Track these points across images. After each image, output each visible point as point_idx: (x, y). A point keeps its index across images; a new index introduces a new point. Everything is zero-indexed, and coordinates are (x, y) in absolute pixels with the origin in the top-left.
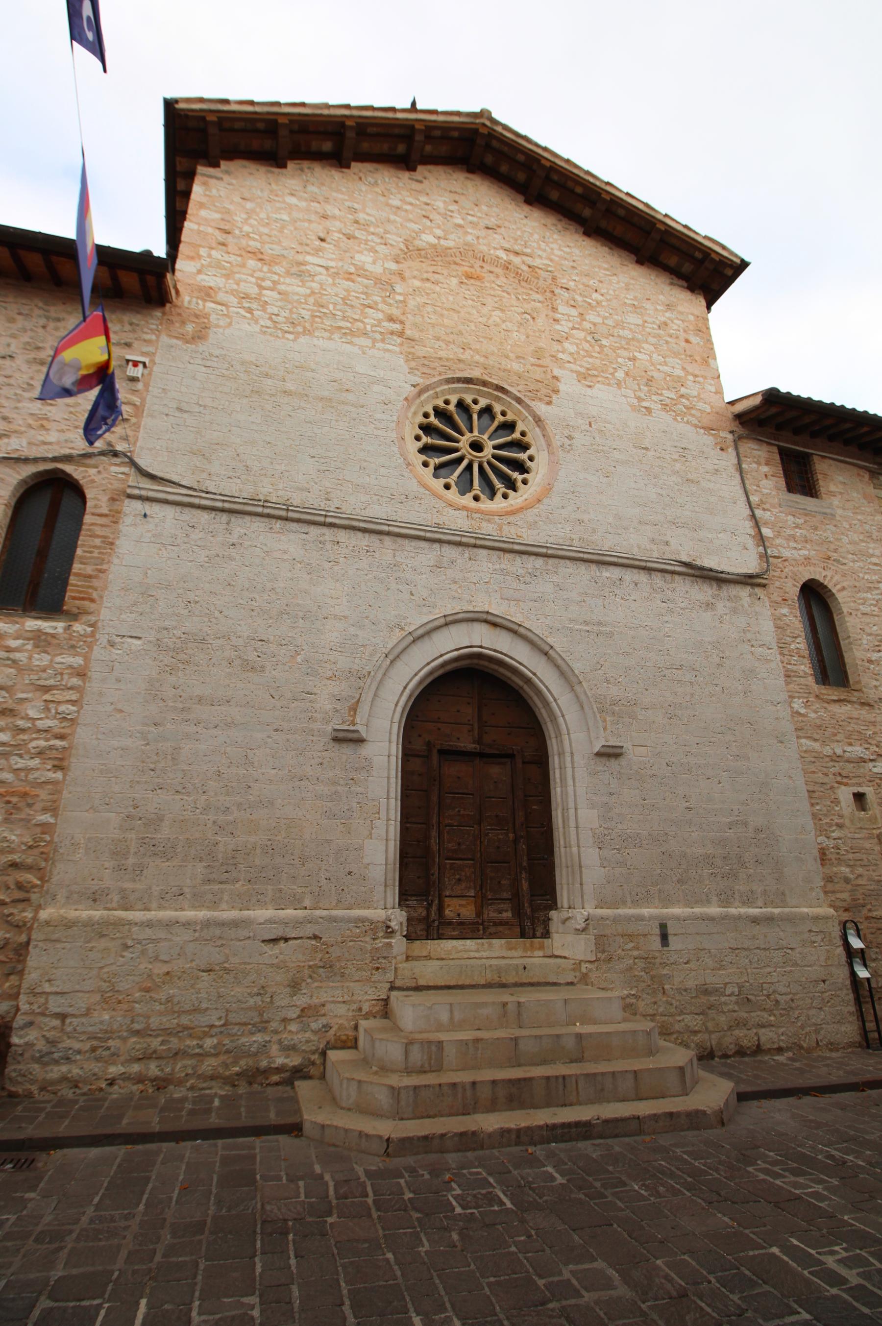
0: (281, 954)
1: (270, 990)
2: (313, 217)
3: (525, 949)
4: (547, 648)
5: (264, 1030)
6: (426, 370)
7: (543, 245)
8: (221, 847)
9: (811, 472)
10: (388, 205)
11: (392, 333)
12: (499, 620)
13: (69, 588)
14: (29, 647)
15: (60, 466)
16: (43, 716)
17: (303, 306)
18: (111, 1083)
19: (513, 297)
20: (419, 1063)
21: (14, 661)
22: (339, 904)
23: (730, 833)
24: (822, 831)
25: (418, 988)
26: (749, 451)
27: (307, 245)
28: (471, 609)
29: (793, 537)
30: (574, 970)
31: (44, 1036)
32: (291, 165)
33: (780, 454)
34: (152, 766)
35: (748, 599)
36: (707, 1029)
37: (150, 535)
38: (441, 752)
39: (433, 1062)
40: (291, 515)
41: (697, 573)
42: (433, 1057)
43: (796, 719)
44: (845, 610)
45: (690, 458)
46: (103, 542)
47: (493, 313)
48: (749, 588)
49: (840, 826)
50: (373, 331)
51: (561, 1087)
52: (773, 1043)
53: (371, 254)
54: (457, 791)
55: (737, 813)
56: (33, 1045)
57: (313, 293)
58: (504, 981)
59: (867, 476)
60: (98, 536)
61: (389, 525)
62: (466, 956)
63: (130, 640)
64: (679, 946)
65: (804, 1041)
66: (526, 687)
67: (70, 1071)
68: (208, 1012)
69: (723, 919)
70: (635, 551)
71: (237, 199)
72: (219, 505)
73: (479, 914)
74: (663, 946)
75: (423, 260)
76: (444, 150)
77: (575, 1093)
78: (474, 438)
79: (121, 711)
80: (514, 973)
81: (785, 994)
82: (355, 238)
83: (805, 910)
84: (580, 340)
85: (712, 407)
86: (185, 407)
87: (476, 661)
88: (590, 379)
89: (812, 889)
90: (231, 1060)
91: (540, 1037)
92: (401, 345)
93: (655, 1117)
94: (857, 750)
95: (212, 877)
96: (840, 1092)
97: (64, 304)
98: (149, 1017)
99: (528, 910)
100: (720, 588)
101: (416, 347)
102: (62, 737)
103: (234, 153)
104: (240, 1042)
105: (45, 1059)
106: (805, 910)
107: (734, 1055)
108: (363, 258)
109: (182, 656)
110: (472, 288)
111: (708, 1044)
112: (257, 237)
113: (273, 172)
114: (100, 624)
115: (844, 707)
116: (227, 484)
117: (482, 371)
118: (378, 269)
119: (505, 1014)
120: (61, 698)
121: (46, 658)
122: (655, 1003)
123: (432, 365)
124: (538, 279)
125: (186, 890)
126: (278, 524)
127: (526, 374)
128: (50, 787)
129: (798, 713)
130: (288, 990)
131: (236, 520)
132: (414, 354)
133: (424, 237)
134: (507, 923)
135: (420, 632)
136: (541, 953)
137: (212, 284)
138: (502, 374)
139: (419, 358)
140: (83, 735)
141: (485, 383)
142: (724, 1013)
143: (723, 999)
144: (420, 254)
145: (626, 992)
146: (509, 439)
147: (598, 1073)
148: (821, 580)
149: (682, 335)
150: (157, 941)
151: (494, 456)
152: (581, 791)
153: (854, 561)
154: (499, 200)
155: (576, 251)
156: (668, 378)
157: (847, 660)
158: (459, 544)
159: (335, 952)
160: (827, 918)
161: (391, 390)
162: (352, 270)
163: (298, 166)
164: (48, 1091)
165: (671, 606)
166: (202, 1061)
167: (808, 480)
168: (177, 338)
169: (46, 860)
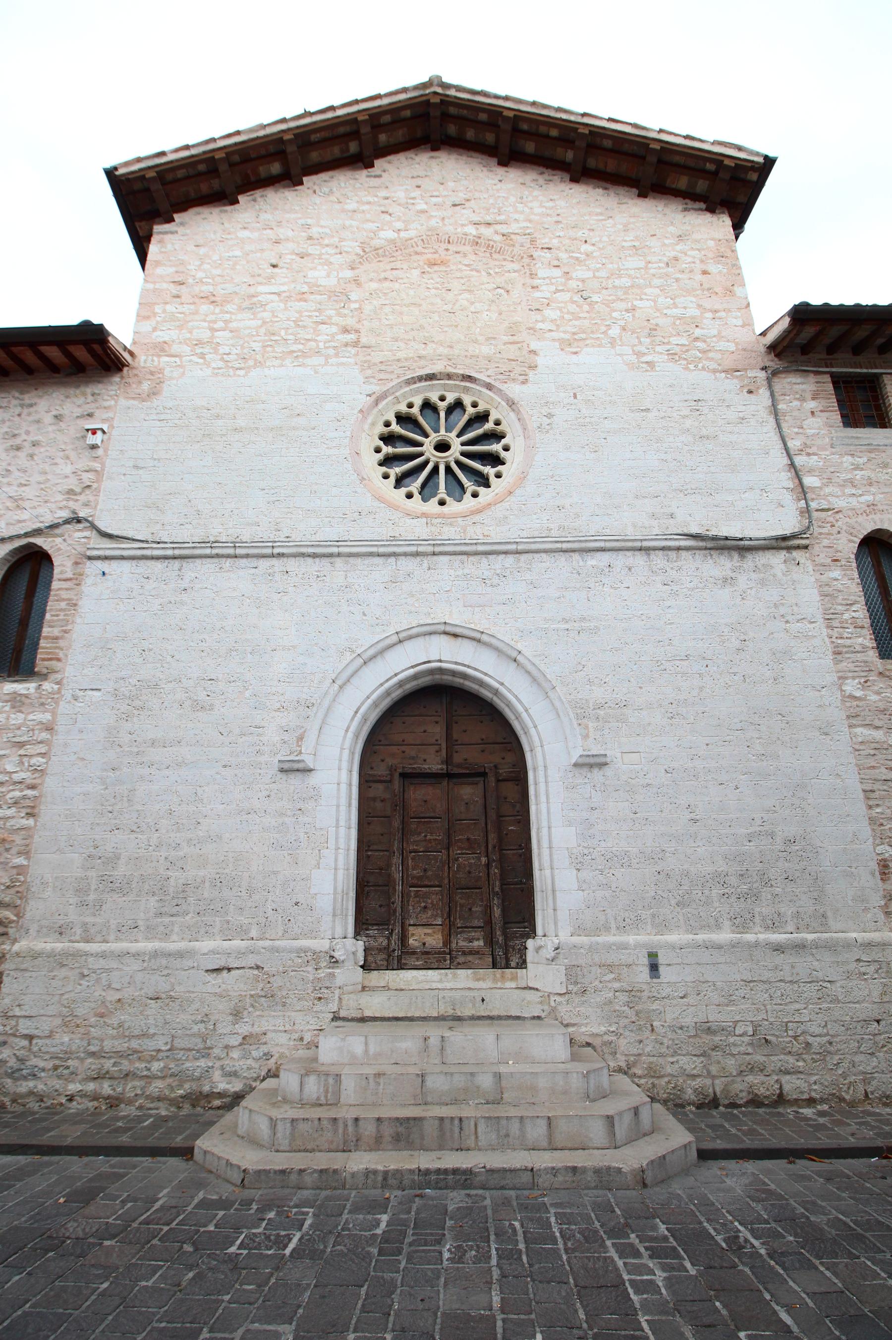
0: (223, 983)
1: (213, 1018)
3: (495, 980)
4: (514, 654)
6: (382, 376)
7: (520, 207)
9: (883, 396)
10: (343, 211)
11: (346, 345)
12: (458, 631)
13: (40, 651)
14: (7, 708)
16: (18, 769)
17: (254, 339)
18: (71, 1099)
19: (484, 273)
20: (315, 1096)
23: (751, 847)
25: (363, 1020)
26: (788, 387)
27: (259, 275)
29: (852, 483)
31: (15, 1054)
34: (110, 808)
35: (783, 566)
36: (709, 1072)
38: (403, 775)
39: (329, 1095)
40: (239, 551)
41: (710, 544)
42: (330, 1090)
43: (848, 704)
45: (705, 410)
46: (68, 604)
47: (460, 297)
48: (784, 552)
50: (326, 348)
51: (457, 1130)
52: (802, 1092)
53: (326, 267)
56: (6, 1062)
57: (264, 323)
58: (459, 1014)
60: (64, 600)
61: (338, 546)
62: (427, 987)
63: (90, 693)
64: (673, 979)
65: (847, 1092)
66: (495, 699)
67: (36, 1087)
68: (156, 1038)
71: (191, 248)
72: (170, 553)
73: (447, 942)
74: (651, 978)
75: (381, 259)
76: (400, 134)
77: (473, 1137)
79: (83, 759)
80: (471, 1005)
81: (820, 1036)
82: (309, 255)
84: (566, 303)
85: (737, 344)
86: (141, 464)
87: (437, 677)
88: (576, 344)
89: (866, 910)
92: (357, 354)
96: (853, 1157)
97: (36, 389)
98: (102, 1040)
99: (500, 939)
100: (742, 557)
101: (373, 353)
102: (33, 787)
103: (184, 205)
104: (184, 1066)
105: (16, 1075)
106: (854, 935)
109: (137, 703)
110: (435, 276)
111: (711, 1090)
112: (210, 281)
113: (226, 211)
114: (65, 681)
117: (445, 364)
118: (332, 282)
122: (641, 1042)
123: (390, 369)
124: (514, 246)
125: (140, 923)
126: (228, 563)
127: (498, 355)
128: (23, 832)
129: (852, 697)
130: (230, 1018)
131: (187, 565)
132: (369, 361)
133: (382, 234)
134: (477, 953)
136: (513, 985)
137: (166, 339)
139: (375, 364)
140: (50, 784)
141: (449, 376)
143: (732, 1040)
144: (377, 254)
145: (603, 1029)
149: (699, 267)
150: (109, 971)
154: (468, 171)
155: (562, 203)
156: (678, 322)
159: (277, 982)
160: (884, 945)
161: (349, 406)
162: (305, 289)
163: (251, 198)
164: (18, 1103)
165: (675, 588)
166: (150, 1083)
167: (878, 408)
168: (133, 398)
169: (21, 898)
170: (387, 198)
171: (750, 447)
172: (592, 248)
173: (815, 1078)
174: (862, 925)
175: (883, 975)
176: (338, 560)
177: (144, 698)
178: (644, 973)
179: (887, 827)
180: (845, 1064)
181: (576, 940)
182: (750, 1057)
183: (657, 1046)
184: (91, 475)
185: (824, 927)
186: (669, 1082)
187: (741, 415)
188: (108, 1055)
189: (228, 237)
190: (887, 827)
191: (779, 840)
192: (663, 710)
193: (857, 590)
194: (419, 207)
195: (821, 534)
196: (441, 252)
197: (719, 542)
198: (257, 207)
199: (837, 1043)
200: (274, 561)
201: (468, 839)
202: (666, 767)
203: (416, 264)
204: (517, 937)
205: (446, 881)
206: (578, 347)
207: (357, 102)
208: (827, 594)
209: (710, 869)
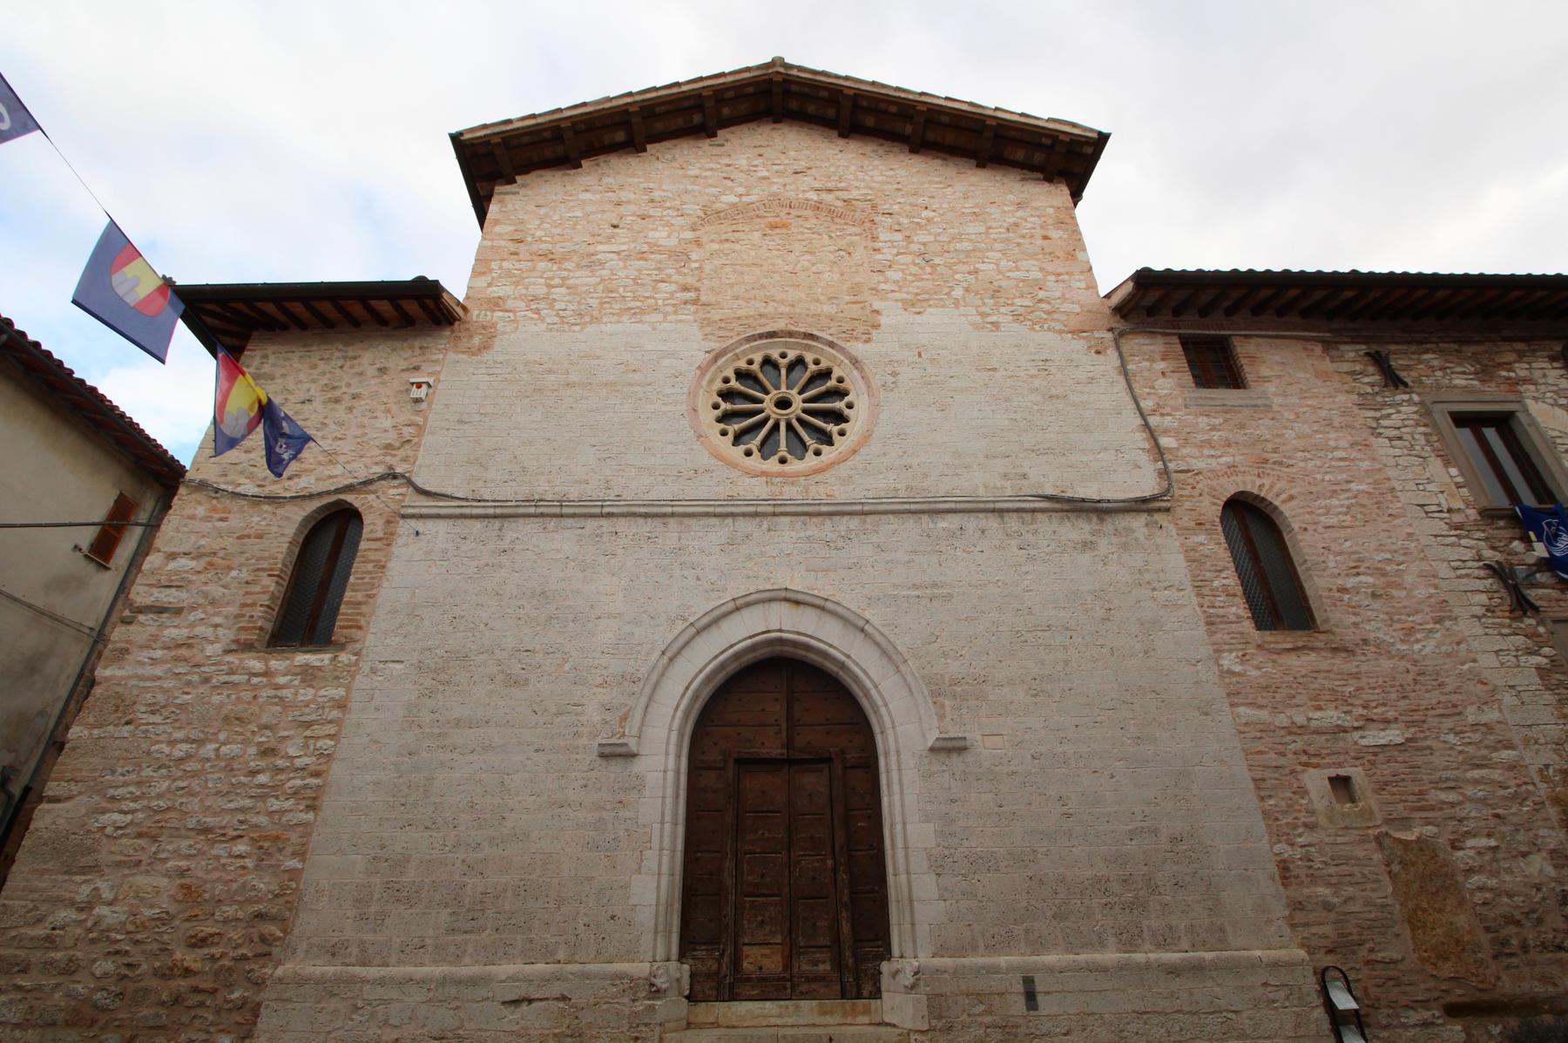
2: (607, 207)
3: (845, 1015)
4: (861, 623)
6: (722, 333)
7: (861, 175)
10: (686, 176)
11: (686, 303)
12: (800, 597)
21: (281, 698)
24: (1277, 835)
28: (769, 587)
33: (1183, 344)
35: (1144, 530)
38: (738, 761)
41: (1066, 507)
44: (1296, 526)
49: (1311, 827)
59: (1318, 349)
64: (1054, 1010)
70: (981, 491)
72: (491, 511)
73: (788, 965)
76: (743, 108)
78: (782, 399)
79: (377, 742)
83: (1258, 953)
89: (1269, 922)
92: (696, 312)
94: (1331, 716)
100: (1102, 520)
102: (317, 774)
103: (527, 167)
106: (1258, 953)
108: (657, 234)
109: (443, 677)
115: (1304, 658)
116: (501, 487)
118: (673, 242)
120: (320, 733)
121: (311, 691)
123: (730, 326)
125: (428, 941)
126: (552, 523)
129: (1230, 672)
131: (509, 525)
133: (725, 199)
135: (705, 621)
136: (866, 1020)
138: (810, 320)
140: (337, 770)
141: (791, 334)
146: (823, 388)
148: (1256, 491)
149: (1039, 232)
151: (805, 411)
152: (910, 798)
153: (1306, 460)
155: (902, 172)
157: (1309, 592)
158: (756, 515)
159: (587, 1017)
162: (645, 248)
176: (672, 521)
178: (1018, 1005)
181: (938, 962)
185: (1223, 944)
200: (603, 522)
207: (701, 79)
208: (1194, 559)
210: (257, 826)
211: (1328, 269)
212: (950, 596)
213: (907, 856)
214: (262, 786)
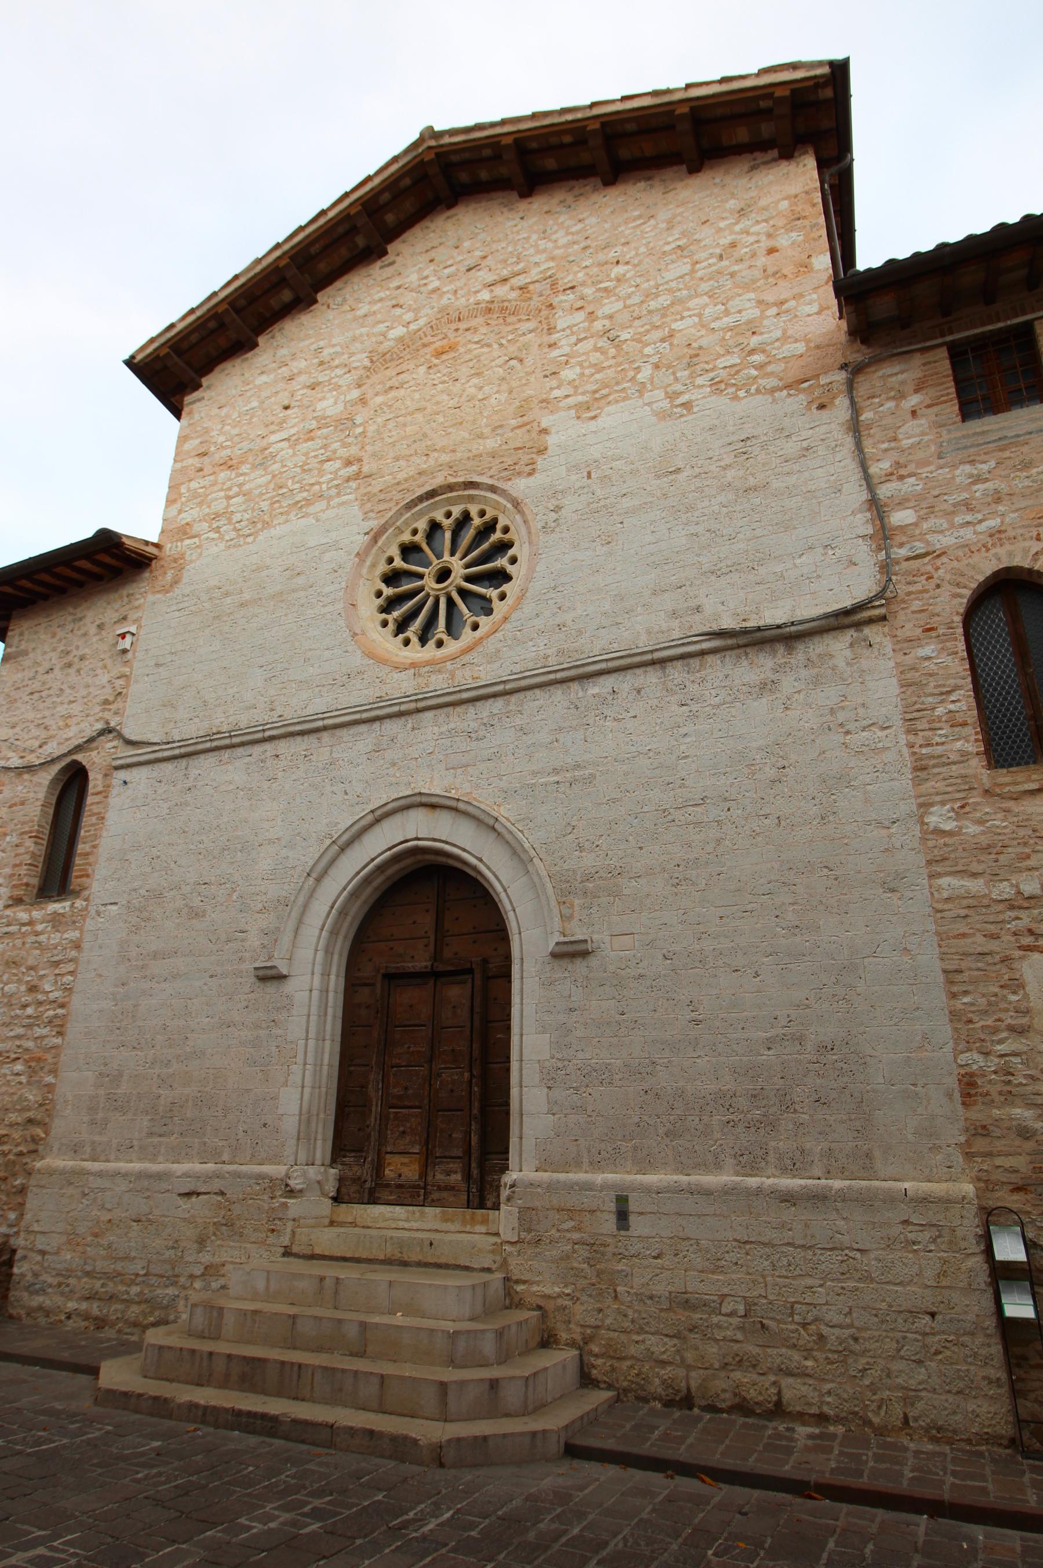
3: (464, 1223)
4: (491, 822)
5: (175, 1284)
8: (162, 1101)
11: (348, 480)
12: (434, 800)
14: (49, 929)
15: (75, 757)
17: (264, 497)
19: (495, 346)
20: (200, 1327)
21: (40, 943)
22: (253, 1159)
24: (967, 1041)
27: (272, 423)
29: (968, 506)
30: (493, 1252)
32: (261, 340)
34: (118, 1025)
35: (848, 653)
36: (683, 1360)
37: (128, 801)
40: (235, 740)
41: (741, 641)
43: (930, 844)
45: (756, 450)
48: (852, 632)
52: (809, 1404)
54: (407, 1023)
55: (784, 1023)
58: (406, 1259)
61: (323, 719)
62: (394, 1226)
64: (646, 1231)
69: (726, 1193)
72: (177, 752)
73: (423, 1175)
74: (619, 1229)
76: (409, 206)
79: (101, 976)
81: (840, 1326)
82: (319, 384)
88: (596, 405)
89: (935, 1148)
90: (148, 1310)
91: (320, 1319)
92: (358, 488)
93: (352, 1431)
95: (155, 1129)
98: (95, 1261)
100: (790, 650)
101: (373, 482)
103: (208, 366)
106: (907, 1185)
107: (730, 1410)
109: (145, 914)
111: (683, 1384)
113: (247, 359)
119: (321, 1289)
122: (600, 1310)
123: (388, 496)
125: (135, 1143)
126: (226, 754)
127: (504, 447)
129: (939, 832)
130: (196, 1246)
131: (194, 762)
132: (369, 493)
135: (345, 837)
136: (483, 1229)
139: (375, 495)
140: (76, 1002)
141: (451, 488)
142: (716, 1340)
143: (715, 1319)
144: (385, 360)
145: (557, 1289)
147: (338, 1369)
148: (1026, 564)
150: (103, 1190)
154: (487, 219)
155: (593, 220)
158: (400, 714)
159: (237, 1209)
160: (949, 1201)
162: (314, 424)
165: (695, 707)
166: (129, 1307)
168: (159, 592)
169: (49, 1116)
170: (399, 287)
171: (813, 488)
172: (626, 268)
173: (828, 1386)
174: (927, 1171)
175: (943, 1247)
177: (150, 908)
178: (609, 1223)
179: (977, 1025)
180: (875, 1373)
182: (739, 1345)
183: (620, 1318)
184: (121, 682)
185: (869, 1171)
186: (632, 1367)
187: (805, 444)
188: (98, 1276)
189: (247, 388)
190: (977, 1025)
191: (809, 1047)
192: (666, 875)
193: (960, 669)
194: (430, 287)
195: (909, 594)
196: (451, 335)
197: (754, 635)
198: (275, 344)
199: (865, 1340)
201: (453, 1050)
202: (664, 951)
203: (423, 360)
204: (495, 1171)
205: (426, 1101)
206: (598, 408)
207: (346, 195)
208: (910, 683)
209: (712, 1087)
210: (27, 1050)
211: (955, 236)
212: (593, 776)
213: (521, 1069)
214: (29, 1017)
